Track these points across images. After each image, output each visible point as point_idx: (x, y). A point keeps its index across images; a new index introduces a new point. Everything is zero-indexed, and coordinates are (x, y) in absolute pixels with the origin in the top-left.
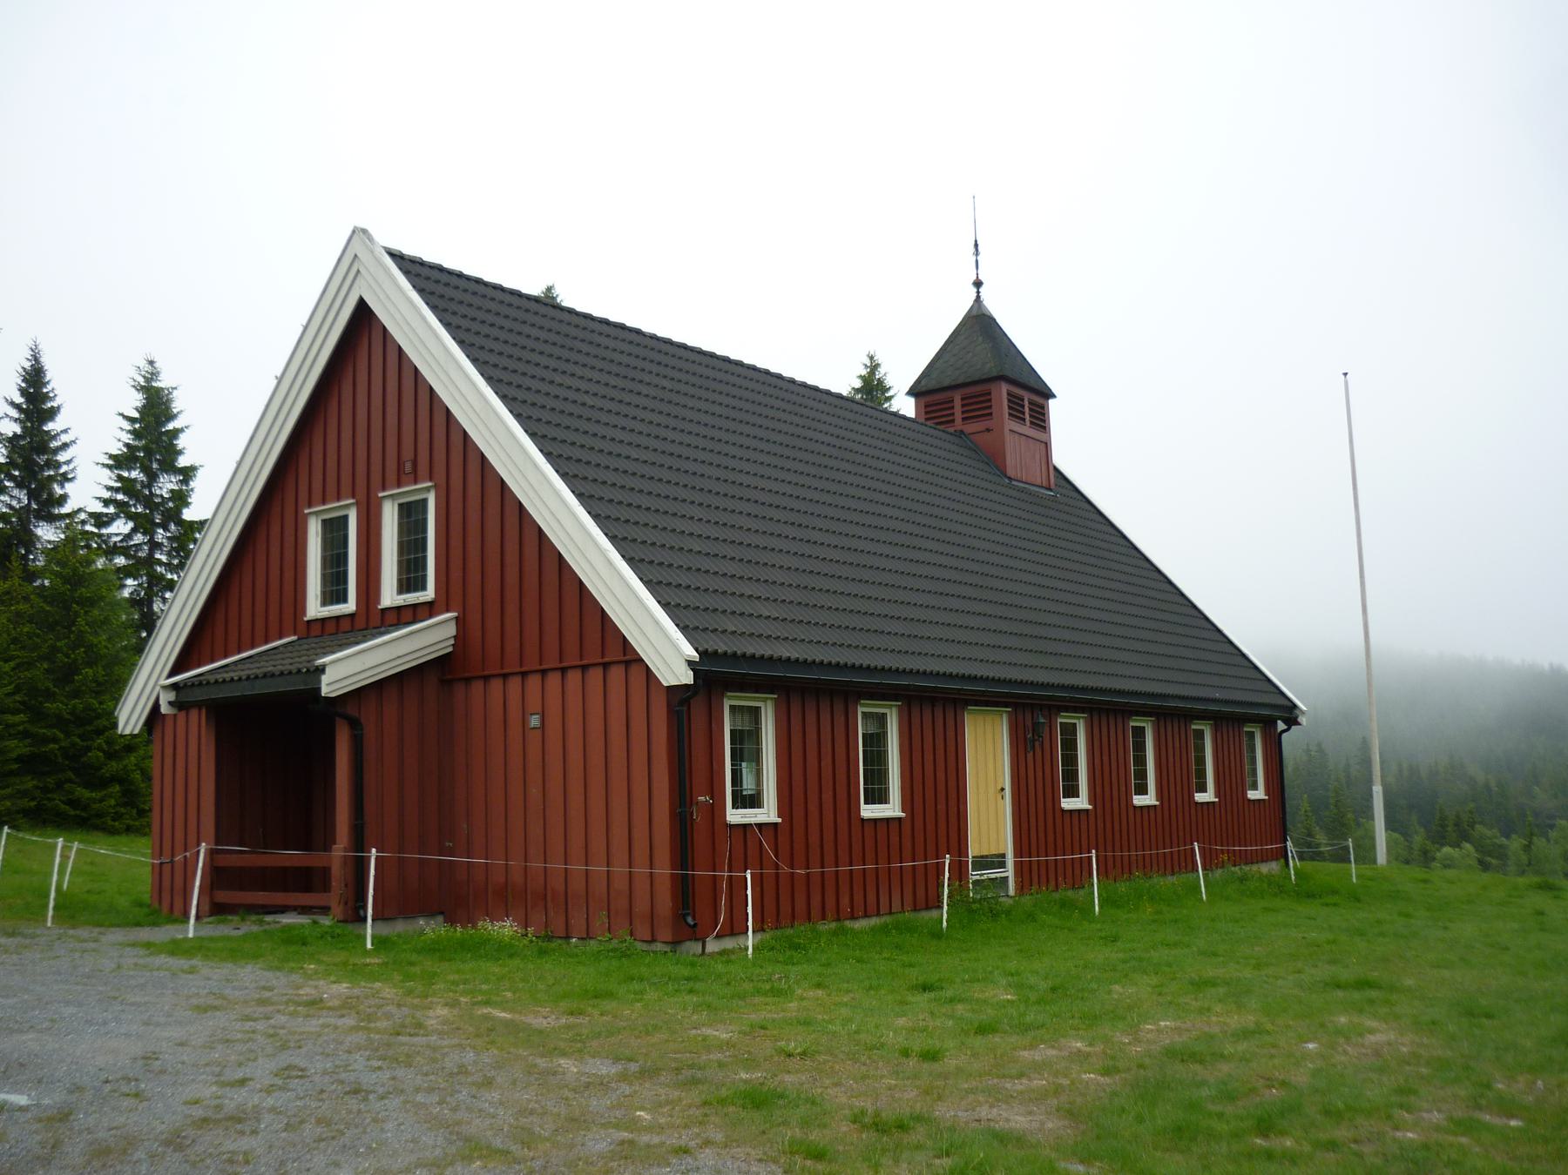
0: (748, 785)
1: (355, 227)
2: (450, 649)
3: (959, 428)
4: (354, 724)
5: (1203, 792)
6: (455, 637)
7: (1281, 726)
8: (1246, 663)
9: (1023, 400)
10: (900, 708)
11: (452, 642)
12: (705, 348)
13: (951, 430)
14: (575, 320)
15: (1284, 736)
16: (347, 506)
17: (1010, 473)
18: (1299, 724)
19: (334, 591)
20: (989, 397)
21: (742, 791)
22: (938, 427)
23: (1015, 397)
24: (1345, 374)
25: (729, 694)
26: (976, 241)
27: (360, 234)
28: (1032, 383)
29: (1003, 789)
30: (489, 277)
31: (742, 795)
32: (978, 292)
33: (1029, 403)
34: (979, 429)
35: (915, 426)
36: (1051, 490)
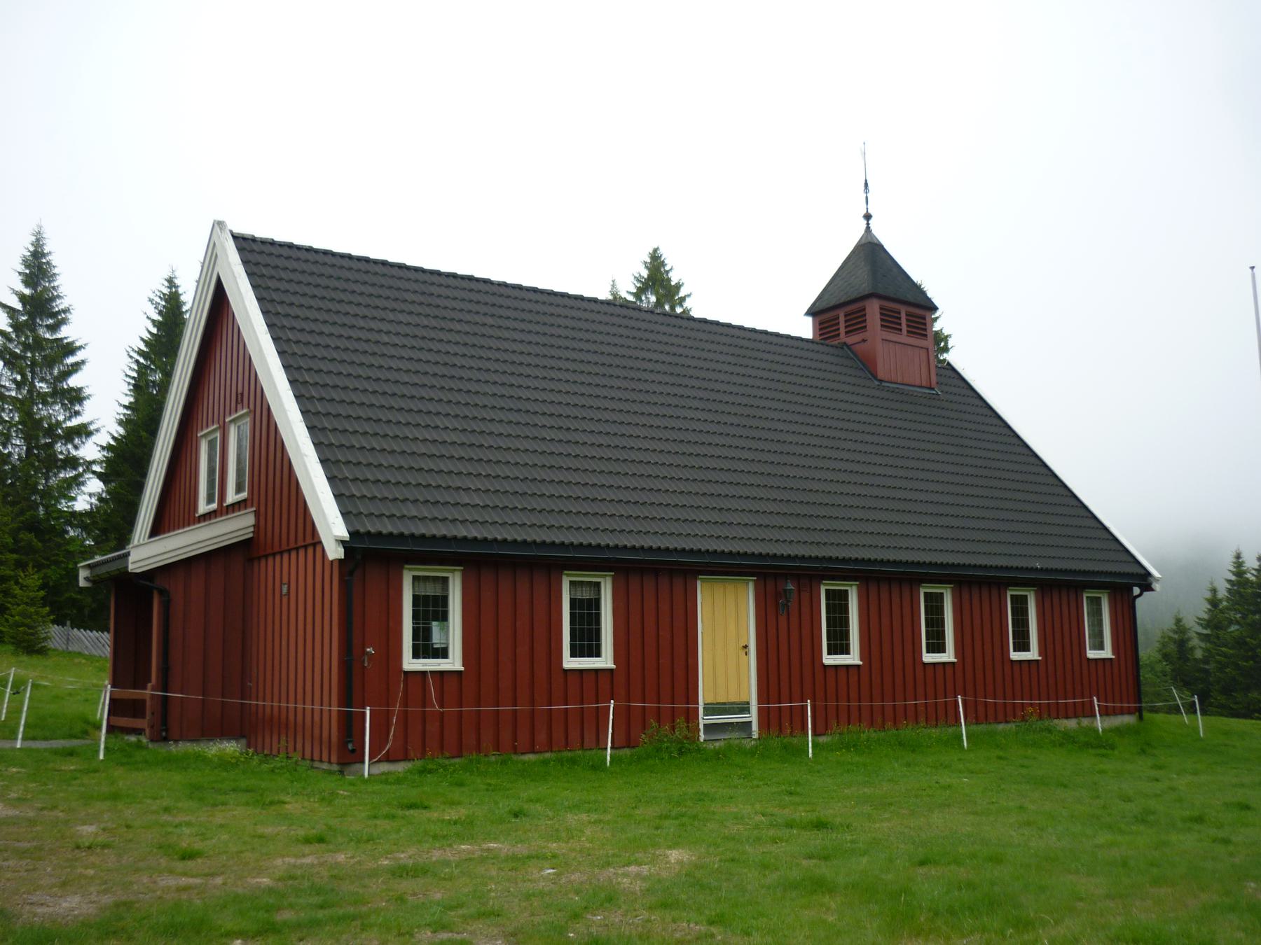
0: (437, 639)
1: (215, 221)
2: (251, 535)
3: (843, 340)
4: (162, 592)
5: (1024, 651)
6: (254, 526)
7: (1136, 591)
8: (1107, 536)
9: (899, 313)
10: (1036, 592)
11: (252, 529)
12: (759, 327)
13: (836, 343)
14: (442, 280)
15: (1138, 601)
16: (214, 430)
17: (881, 375)
18: (1152, 590)
19: (210, 500)
20: (863, 313)
21: (432, 644)
22: (827, 342)
23: (885, 310)
24: (1253, 268)
25: (566, 572)
26: (866, 181)
27: (219, 224)
28: (910, 297)
29: (746, 647)
30: (526, 283)
31: (433, 649)
32: (868, 224)
33: (907, 315)
34: (858, 341)
35: (811, 346)
36: (933, 389)
